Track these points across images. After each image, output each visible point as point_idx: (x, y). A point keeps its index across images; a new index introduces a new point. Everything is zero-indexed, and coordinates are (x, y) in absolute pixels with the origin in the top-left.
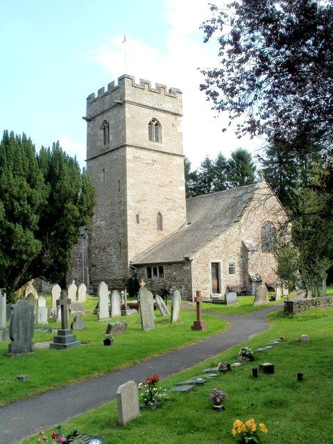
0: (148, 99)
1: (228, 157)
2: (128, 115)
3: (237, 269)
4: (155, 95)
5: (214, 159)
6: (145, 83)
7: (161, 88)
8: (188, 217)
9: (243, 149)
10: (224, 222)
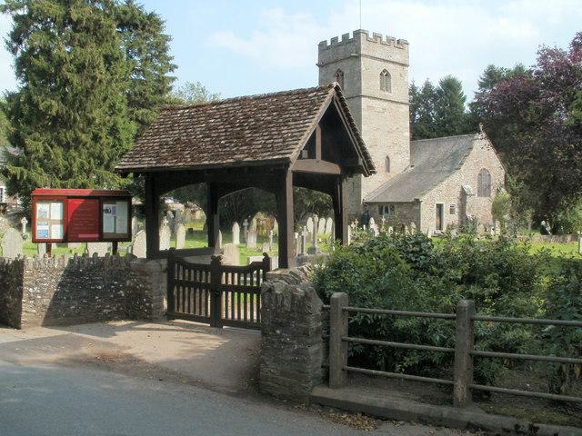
0: (380, 52)
1: (436, 85)
2: (363, 68)
3: (457, 210)
4: (387, 48)
5: (420, 86)
6: (377, 36)
7: (390, 40)
8: (411, 160)
9: (452, 76)
10: (446, 168)
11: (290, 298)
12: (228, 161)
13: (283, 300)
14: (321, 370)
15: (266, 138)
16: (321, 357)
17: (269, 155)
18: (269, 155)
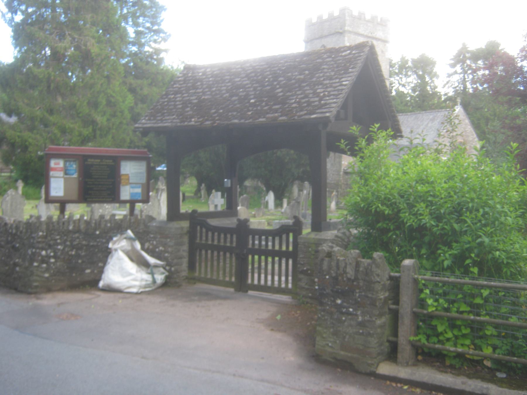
11: (354, 264)
12: (261, 120)
13: (346, 267)
14: (387, 344)
15: (299, 97)
16: (387, 331)
17: (305, 114)
18: (305, 114)
